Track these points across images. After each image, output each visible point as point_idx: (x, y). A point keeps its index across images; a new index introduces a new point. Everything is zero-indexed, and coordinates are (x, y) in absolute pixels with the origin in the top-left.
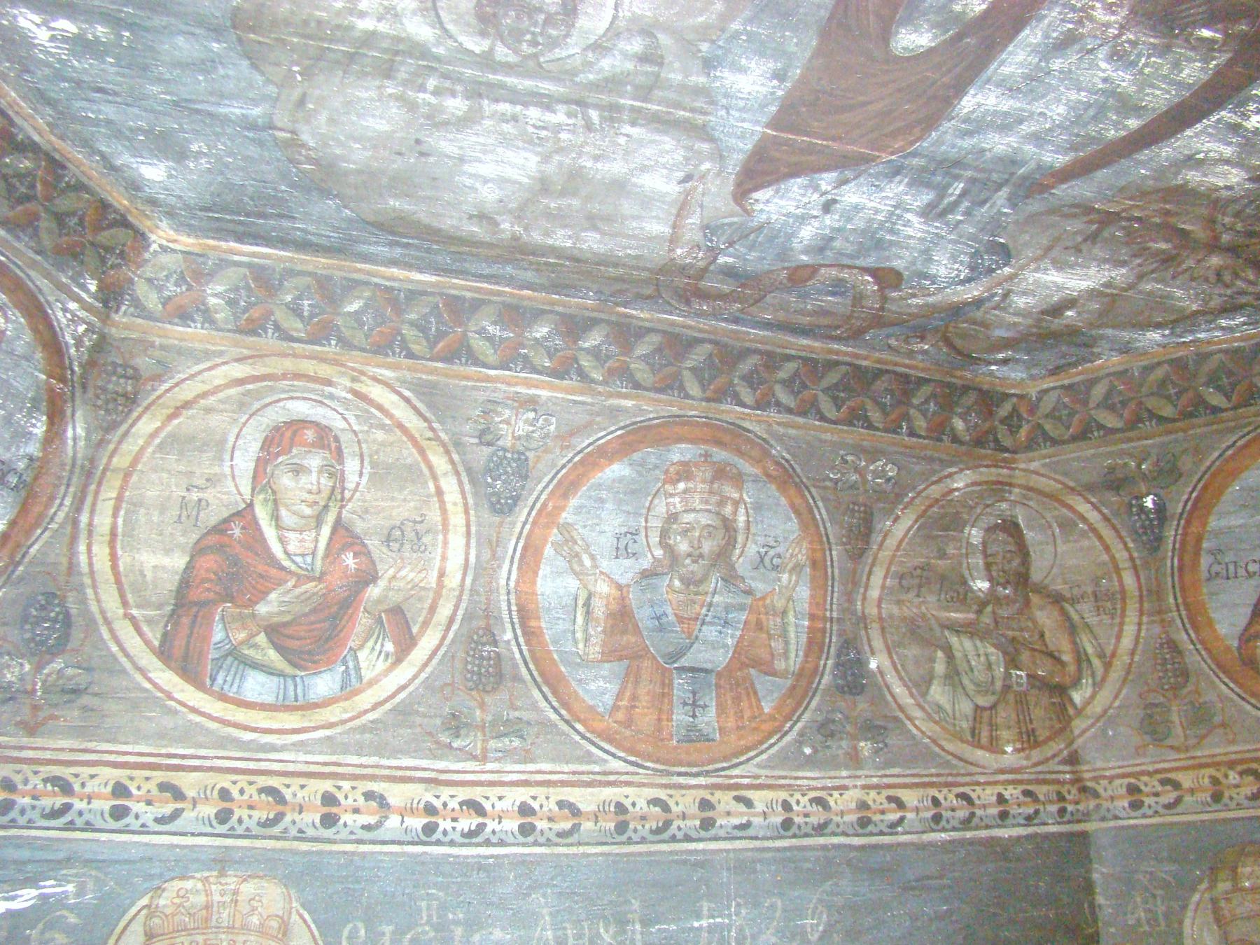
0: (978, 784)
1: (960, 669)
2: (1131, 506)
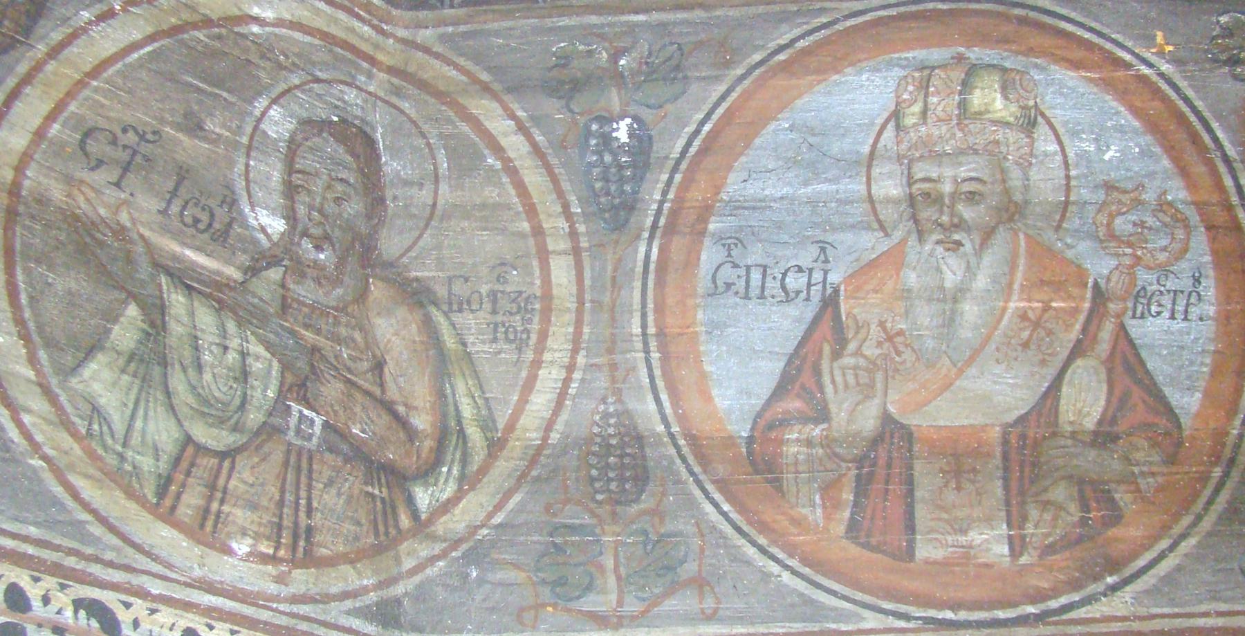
0: (143, 594)
1: (173, 356)
2: (589, 134)
